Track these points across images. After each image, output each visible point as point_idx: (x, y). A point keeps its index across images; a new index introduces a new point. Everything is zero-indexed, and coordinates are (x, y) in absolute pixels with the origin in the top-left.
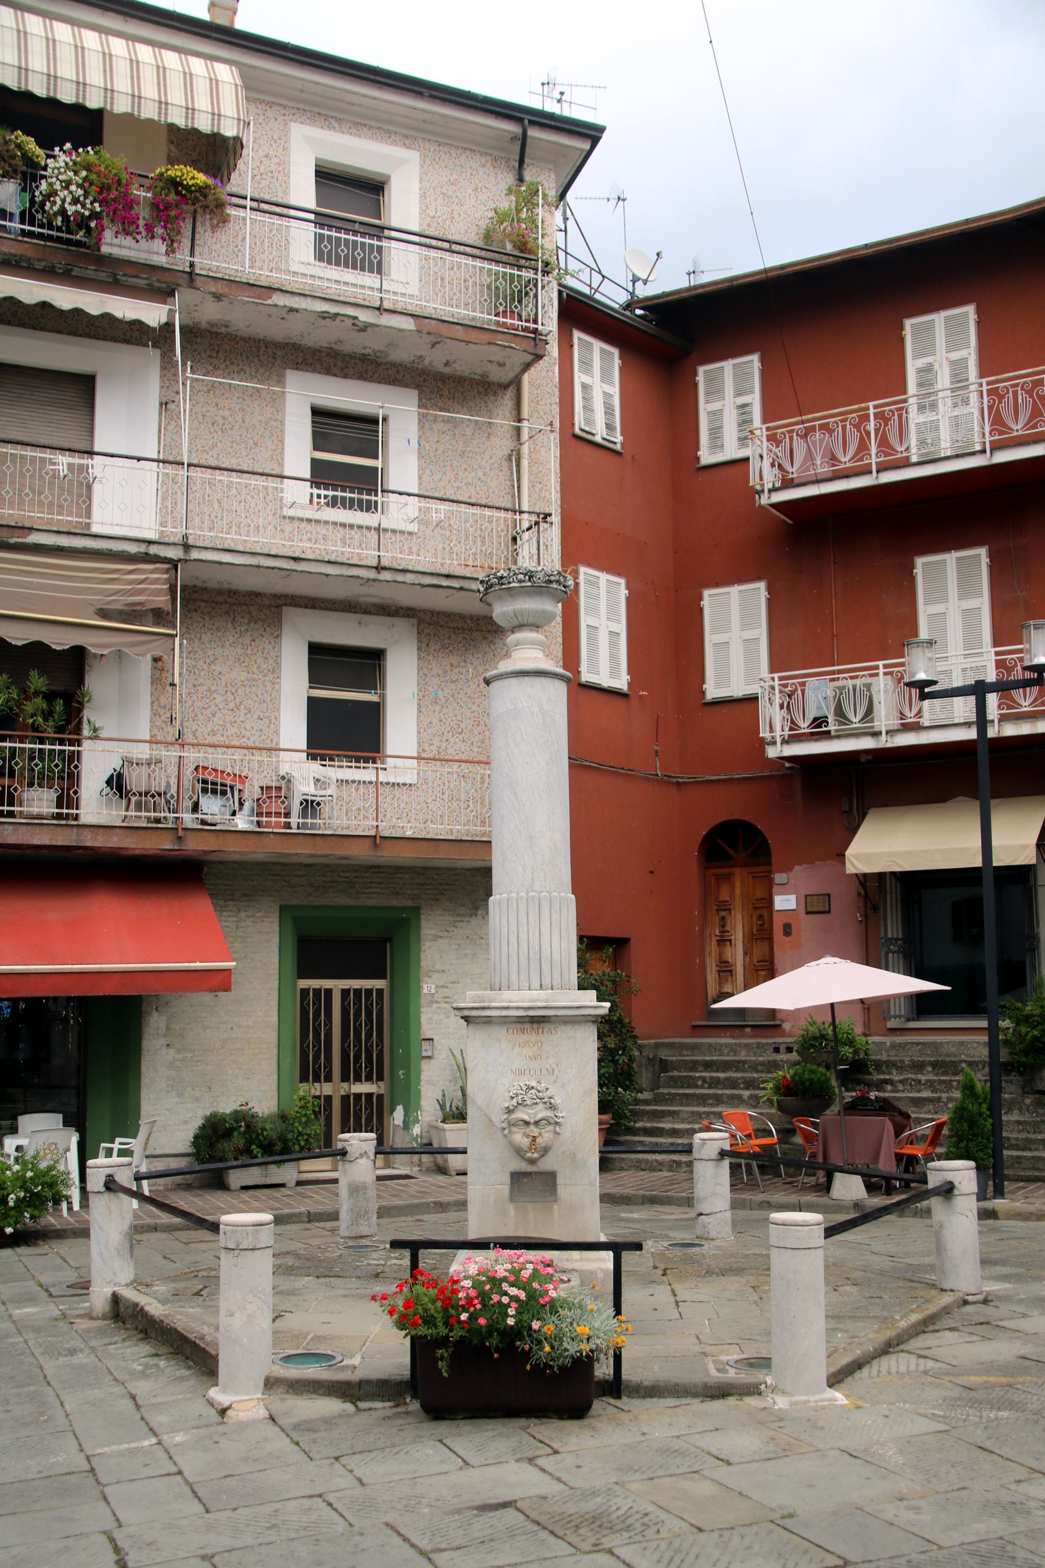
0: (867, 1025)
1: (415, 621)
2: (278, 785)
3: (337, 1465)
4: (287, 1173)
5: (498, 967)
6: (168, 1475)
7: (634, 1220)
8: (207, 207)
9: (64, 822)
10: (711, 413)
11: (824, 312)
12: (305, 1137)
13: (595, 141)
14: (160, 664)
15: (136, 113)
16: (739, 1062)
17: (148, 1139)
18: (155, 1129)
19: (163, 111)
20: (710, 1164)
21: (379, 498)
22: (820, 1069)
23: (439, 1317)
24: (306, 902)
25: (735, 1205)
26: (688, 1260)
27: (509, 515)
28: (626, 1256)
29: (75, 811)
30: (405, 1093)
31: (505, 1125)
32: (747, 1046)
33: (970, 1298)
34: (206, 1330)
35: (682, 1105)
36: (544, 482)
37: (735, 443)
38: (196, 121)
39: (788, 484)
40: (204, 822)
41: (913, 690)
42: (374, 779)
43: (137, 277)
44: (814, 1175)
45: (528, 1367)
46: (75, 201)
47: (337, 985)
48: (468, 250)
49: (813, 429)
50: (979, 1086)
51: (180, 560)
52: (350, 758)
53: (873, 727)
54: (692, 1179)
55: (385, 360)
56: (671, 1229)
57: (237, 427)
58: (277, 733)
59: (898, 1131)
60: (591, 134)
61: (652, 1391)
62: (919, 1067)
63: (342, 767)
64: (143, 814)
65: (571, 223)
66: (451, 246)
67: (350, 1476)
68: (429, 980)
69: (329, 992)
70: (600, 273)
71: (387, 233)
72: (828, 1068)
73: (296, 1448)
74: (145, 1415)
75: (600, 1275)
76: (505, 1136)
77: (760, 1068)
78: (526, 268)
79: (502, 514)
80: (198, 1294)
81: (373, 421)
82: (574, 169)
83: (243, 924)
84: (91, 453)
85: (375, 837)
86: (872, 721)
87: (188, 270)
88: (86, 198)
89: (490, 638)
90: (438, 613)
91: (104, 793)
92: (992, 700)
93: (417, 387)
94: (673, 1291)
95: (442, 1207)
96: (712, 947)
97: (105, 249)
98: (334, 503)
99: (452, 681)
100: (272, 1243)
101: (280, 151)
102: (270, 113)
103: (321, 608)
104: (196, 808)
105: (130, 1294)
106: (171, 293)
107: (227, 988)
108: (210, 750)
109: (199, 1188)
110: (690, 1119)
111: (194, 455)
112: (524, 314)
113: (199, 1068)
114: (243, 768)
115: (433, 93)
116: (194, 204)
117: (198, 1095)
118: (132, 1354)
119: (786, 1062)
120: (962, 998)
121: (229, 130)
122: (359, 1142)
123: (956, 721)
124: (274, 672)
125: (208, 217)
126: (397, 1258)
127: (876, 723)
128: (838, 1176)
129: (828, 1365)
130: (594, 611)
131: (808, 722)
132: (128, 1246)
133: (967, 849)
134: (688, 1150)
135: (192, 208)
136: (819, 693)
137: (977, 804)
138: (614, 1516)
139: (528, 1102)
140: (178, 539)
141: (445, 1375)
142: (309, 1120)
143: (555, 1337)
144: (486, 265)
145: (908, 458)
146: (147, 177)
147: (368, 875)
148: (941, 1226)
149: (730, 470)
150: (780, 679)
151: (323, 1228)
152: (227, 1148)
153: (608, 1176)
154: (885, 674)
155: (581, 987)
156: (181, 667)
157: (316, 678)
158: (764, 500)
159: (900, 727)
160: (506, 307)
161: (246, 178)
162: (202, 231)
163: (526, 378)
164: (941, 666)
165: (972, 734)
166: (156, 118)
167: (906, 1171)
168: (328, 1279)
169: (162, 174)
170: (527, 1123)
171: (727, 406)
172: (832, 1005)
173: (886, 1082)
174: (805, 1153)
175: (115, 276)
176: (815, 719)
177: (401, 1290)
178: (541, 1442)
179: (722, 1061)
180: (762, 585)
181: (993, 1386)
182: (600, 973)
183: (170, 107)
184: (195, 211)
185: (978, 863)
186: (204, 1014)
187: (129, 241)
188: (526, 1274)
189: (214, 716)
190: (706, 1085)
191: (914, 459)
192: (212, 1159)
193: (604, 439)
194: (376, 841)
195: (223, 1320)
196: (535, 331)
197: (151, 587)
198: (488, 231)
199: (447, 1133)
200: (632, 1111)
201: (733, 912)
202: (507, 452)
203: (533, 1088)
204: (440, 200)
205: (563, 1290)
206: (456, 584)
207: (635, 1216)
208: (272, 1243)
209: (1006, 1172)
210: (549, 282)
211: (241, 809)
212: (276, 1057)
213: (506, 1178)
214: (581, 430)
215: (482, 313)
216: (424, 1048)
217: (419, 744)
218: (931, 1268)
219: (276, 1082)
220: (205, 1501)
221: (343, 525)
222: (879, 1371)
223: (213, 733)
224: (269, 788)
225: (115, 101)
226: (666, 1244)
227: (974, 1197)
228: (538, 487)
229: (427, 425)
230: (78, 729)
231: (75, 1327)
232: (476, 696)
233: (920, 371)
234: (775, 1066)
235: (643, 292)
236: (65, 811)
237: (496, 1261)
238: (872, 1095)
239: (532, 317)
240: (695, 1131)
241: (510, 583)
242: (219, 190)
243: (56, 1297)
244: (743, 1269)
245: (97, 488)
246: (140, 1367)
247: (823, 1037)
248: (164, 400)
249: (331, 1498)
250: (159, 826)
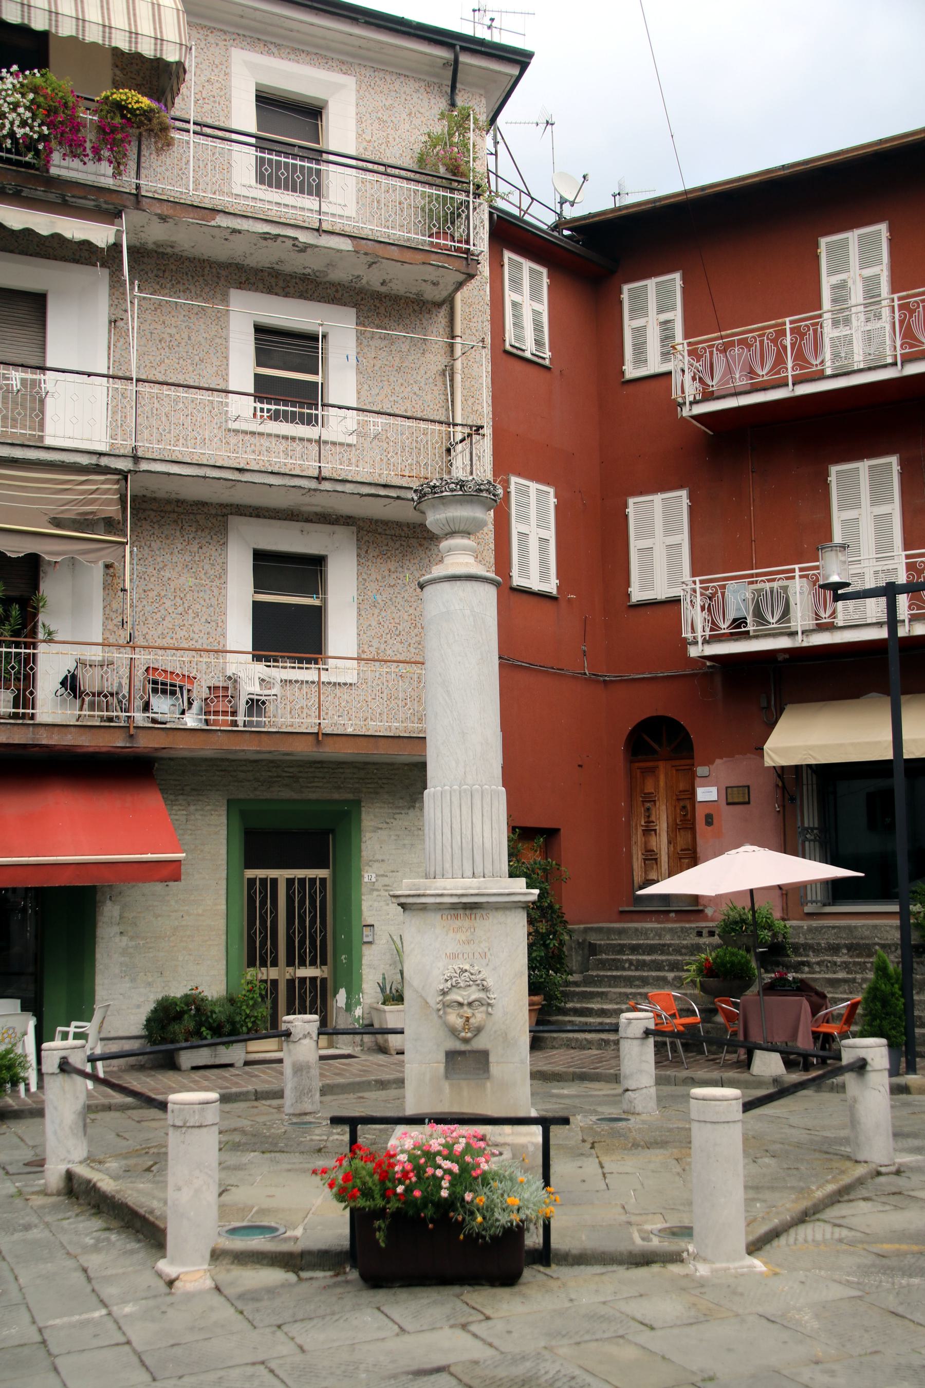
0: (785, 909)
1: (354, 529)
2: (225, 685)
3: (279, 1334)
4: (236, 1053)
5: (433, 857)
6: (117, 1344)
7: (565, 1095)
8: (152, 130)
9: (21, 721)
10: (636, 330)
11: (744, 231)
12: (253, 1019)
13: (524, 66)
14: (112, 570)
15: (81, 37)
16: (664, 945)
17: (102, 1023)
18: (109, 1013)
19: (107, 35)
21: (319, 412)
22: (741, 952)
23: (377, 1190)
24: (252, 796)
25: (660, 1081)
26: (615, 1134)
27: (443, 428)
28: (554, 1130)
29: (31, 711)
30: (348, 976)
31: (440, 1006)
32: (671, 930)
33: (883, 1170)
34: (155, 1204)
35: (610, 986)
36: (476, 397)
37: (658, 358)
38: (139, 46)
39: (708, 396)
40: (154, 721)
41: (828, 592)
42: (316, 679)
43: (85, 198)
44: (736, 1052)
45: (462, 1237)
46: (24, 124)
47: (282, 875)
48: (403, 173)
49: (732, 344)
50: (891, 968)
51: (130, 471)
52: (293, 659)
53: (789, 627)
54: (618, 1057)
55: (324, 280)
56: (599, 1104)
57: (183, 344)
58: (224, 635)
59: (815, 1011)
60: (520, 59)
61: (581, 1259)
62: (834, 949)
63: (286, 668)
64: (96, 713)
65: (501, 147)
66: (387, 169)
67: (292, 1345)
68: (370, 869)
69: (274, 881)
70: (529, 195)
71: (325, 156)
72: (748, 951)
73: (240, 1317)
74: (97, 1287)
75: (531, 1149)
76: (440, 1017)
77: (683, 951)
78: (458, 190)
79: (437, 427)
80: (149, 1169)
81: (313, 338)
82: (504, 94)
83: (193, 817)
84: (43, 369)
85: (317, 733)
86: (789, 621)
87: (134, 191)
88: (34, 120)
89: (426, 544)
90: (377, 521)
91: (59, 694)
92: (903, 601)
93: (355, 305)
94: (600, 1163)
95: (382, 1085)
96: (638, 837)
97: (54, 171)
98: (276, 416)
99: (390, 586)
100: (217, 1120)
101: (222, 75)
102: (211, 39)
103: (265, 517)
104: (146, 707)
105: (83, 1171)
106: (118, 215)
107: (177, 878)
108: (160, 652)
109: (151, 1068)
110: (618, 1000)
111: (142, 371)
112: (457, 235)
113: (151, 955)
114: (191, 669)
115: (367, 19)
116: (139, 127)
117: (150, 980)
118: (86, 1228)
119: (708, 945)
120: (875, 884)
121: (171, 56)
122: (303, 1024)
123: (869, 621)
124: (220, 577)
125: (153, 140)
126: (338, 1134)
127: (792, 624)
128: (758, 1054)
129: (747, 1233)
130: (524, 518)
131: (727, 624)
132: (81, 1124)
133: (879, 742)
134: (615, 1029)
135: (138, 131)
136: (738, 596)
137: (888, 700)
138: (542, 1380)
139: (462, 984)
140: (128, 451)
141: (383, 1245)
142: (256, 1003)
143: (487, 1207)
144: (420, 188)
145: (823, 371)
146: (93, 100)
147: (312, 770)
148: (855, 1100)
149: (654, 383)
150: (701, 582)
151: (269, 1106)
152: (178, 1031)
153: (539, 1054)
154: (801, 577)
155: (511, 875)
156: (132, 574)
157: (260, 584)
158: (686, 412)
159: (815, 627)
160: (439, 228)
161: (188, 103)
162: (147, 154)
163: (459, 296)
164: (854, 569)
165: (882, 633)
166: (100, 42)
167: (823, 1048)
168: (273, 1155)
169: (107, 98)
170: (461, 1004)
171: (650, 323)
172: (751, 891)
173: (803, 963)
174: (727, 1031)
175: (63, 197)
176: (735, 620)
177: (341, 1165)
178: (473, 1308)
179: (648, 945)
180: (684, 493)
181: (905, 1254)
182: (532, 861)
183: (113, 31)
184: (140, 134)
185: (889, 755)
186: (156, 903)
187: (76, 164)
188: (459, 1148)
189: (164, 620)
190: (633, 968)
191: (829, 372)
192: (164, 1041)
193: (533, 354)
194: (318, 737)
195: (171, 1194)
196: (467, 251)
197: (102, 496)
198: (422, 154)
199: (388, 1015)
200: (562, 992)
201: (657, 803)
202: (441, 367)
203: (466, 971)
204: (376, 125)
205: (495, 1163)
206: (393, 493)
207: (566, 1092)
208: (217, 1120)
209: (918, 1049)
210: (480, 204)
211: (189, 708)
212: (224, 943)
213: (442, 1057)
214: (512, 346)
215: (417, 234)
216: (365, 933)
217: (359, 645)
218: (846, 1141)
219: (224, 967)
220: (152, 1370)
221: (286, 438)
222: (796, 1239)
223: (163, 636)
224: (216, 688)
225: (60, 24)
226: (594, 1118)
227: (886, 1074)
228: (471, 401)
229: (365, 342)
230: (34, 633)
231: (30, 1203)
232: (413, 600)
233: (834, 287)
234: (698, 949)
235: (570, 213)
236: (21, 711)
237: (431, 1135)
238: (790, 976)
239: (464, 237)
240: (622, 1011)
241: (442, 492)
242: (163, 114)
243: (13, 1174)
244: (667, 1142)
245: (49, 401)
246: (92, 1241)
247: (743, 921)
248: (113, 317)
249: (273, 1365)
250: (112, 724)
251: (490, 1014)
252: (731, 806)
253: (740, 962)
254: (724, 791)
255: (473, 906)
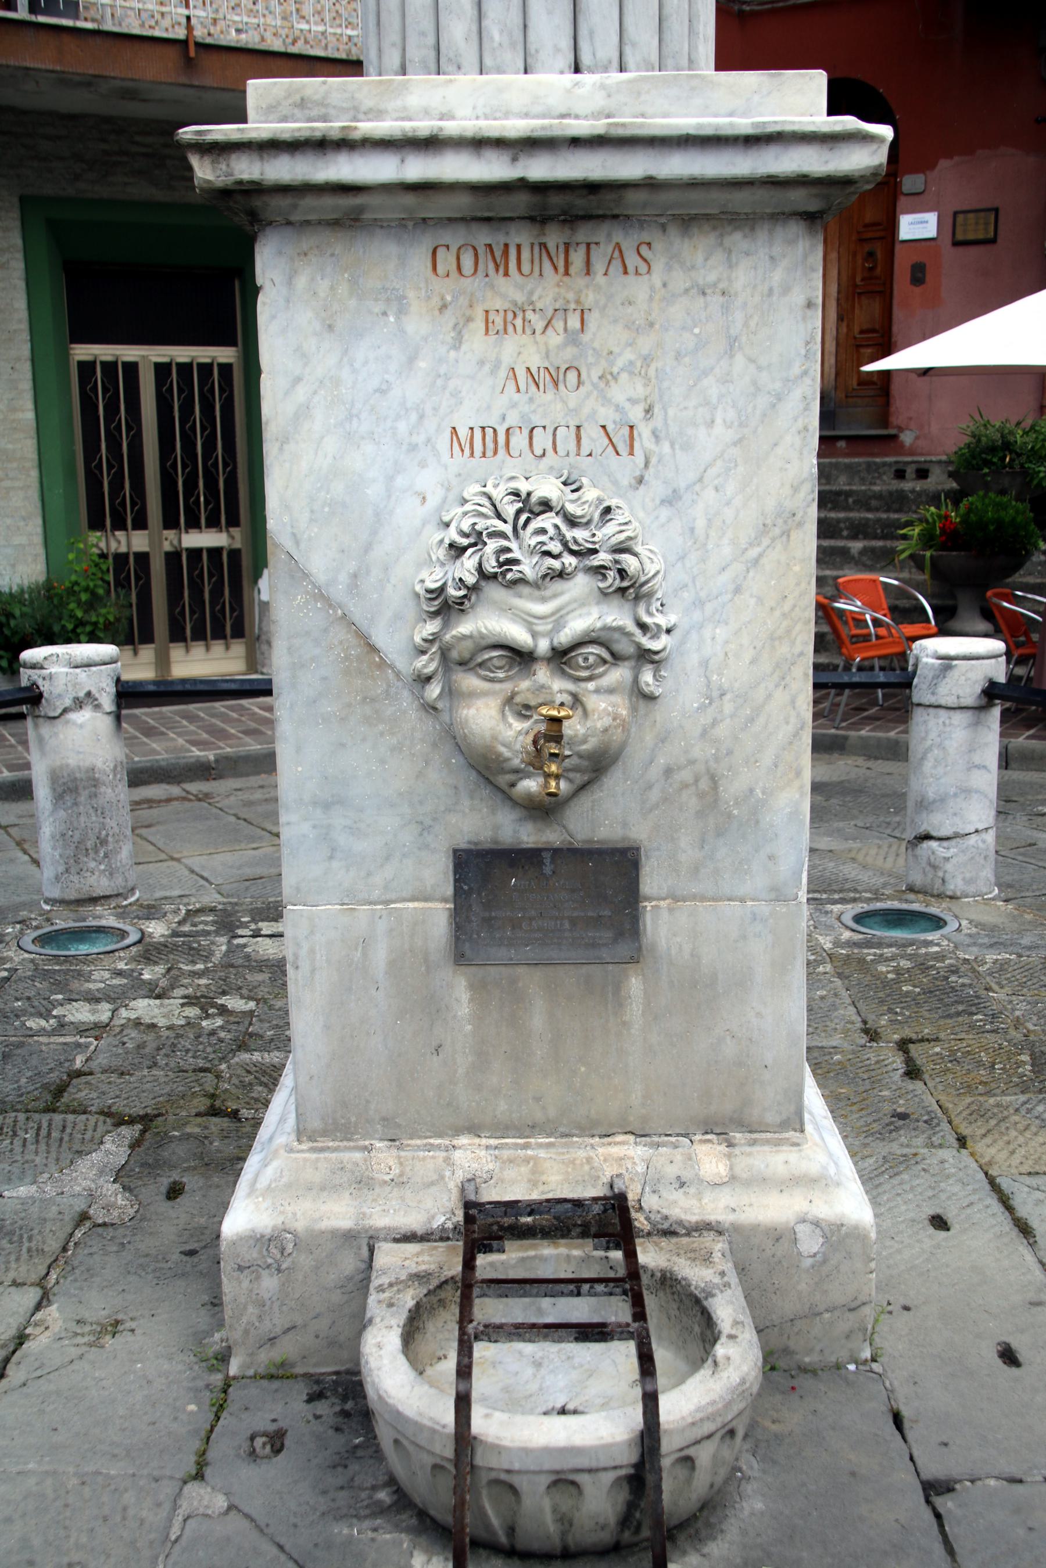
16: (838, 493)
20: (959, 719)
32: (849, 467)
69: (132, 368)
76: (431, 709)
77: (874, 503)
139: (529, 567)
170: (520, 657)
203: (546, 506)
213: (437, 873)
219: (39, 530)
251: (650, 698)
252: (961, 250)
253: (1014, 519)
254: (950, 221)
255: (581, 203)
